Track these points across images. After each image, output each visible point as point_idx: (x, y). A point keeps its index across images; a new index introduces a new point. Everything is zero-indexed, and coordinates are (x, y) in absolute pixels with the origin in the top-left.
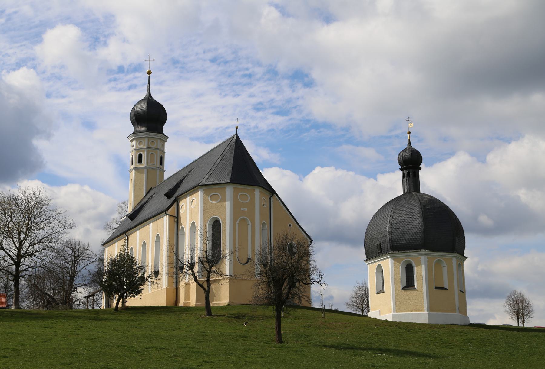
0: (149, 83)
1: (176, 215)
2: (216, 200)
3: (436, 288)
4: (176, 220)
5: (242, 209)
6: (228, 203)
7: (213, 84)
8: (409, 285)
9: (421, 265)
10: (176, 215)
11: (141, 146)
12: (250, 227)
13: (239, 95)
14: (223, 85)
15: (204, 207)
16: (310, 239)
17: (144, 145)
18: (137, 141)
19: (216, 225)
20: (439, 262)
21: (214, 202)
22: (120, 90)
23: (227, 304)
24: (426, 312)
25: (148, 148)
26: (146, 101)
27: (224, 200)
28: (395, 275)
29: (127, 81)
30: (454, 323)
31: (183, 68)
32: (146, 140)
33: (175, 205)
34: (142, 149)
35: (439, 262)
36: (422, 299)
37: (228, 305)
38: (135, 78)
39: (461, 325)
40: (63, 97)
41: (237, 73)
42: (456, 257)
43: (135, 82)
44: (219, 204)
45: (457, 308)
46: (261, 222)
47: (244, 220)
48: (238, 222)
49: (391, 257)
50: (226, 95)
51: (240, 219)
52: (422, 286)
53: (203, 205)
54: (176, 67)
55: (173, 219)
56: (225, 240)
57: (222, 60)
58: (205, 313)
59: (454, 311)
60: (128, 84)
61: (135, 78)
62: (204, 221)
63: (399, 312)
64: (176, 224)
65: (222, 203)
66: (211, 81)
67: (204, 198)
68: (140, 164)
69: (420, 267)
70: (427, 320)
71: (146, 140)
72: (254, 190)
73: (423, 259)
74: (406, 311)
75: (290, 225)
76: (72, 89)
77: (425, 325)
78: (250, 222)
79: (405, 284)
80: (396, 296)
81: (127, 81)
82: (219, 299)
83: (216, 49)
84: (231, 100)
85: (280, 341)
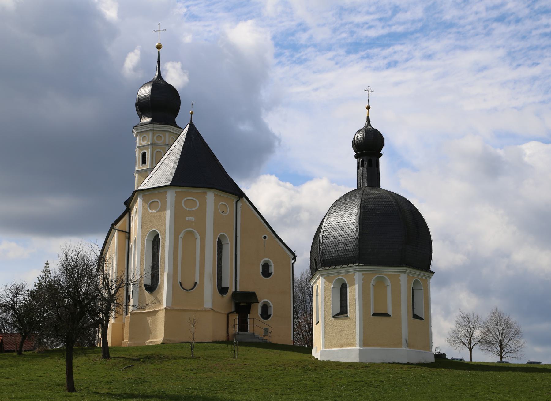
0: (159, 61)
1: (127, 231)
2: (155, 209)
3: (374, 315)
4: (127, 236)
5: (187, 219)
6: (168, 212)
7: (501, 52)
8: (343, 312)
9: (355, 284)
10: (127, 231)
11: (145, 143)
12: (198, 241)
13: (538, 64)
14: (514, 52)
15: (143, 217)
16: (293, 253)
17: (148, 141)
18: (140, 136)
19: (156, 241)
20: (380, 281)
21: (154, 211)
22: (377, 69)
23: (161, 341)
24: (358, 347)
25: (153, 144)
26: (151, 84)
27: (164, 209)
28: (325, 299)
29: (385, 58)
30: (400, 362)
31: (459, 33)
32: (150, 134)
33: (127, 216)
34: (145, 147)
35: (380, 281)
36: (355, 330)
37: (163, 343)
38: (395, 52)
39: (408, 364)
40: (304, 84)
41: (534, 33)
42: (405, 272)
43: (396, 57)
44: (158, 213)
45: (404, 341)
46: (215, 234)
47: (190, 233)
48: (182, 235)
49: (321, 275)
50: (519, 65)
51: (185, 231)
52: (355, 313)
53: (141, 216)
54: (450, 33)
55: (123, 235)
56: (164, 260)
57: (512, 17)
58: (101, 355)
59: (399, 344)
60: (386, 61)
61: (395, 52)
62: (142, 237)
63: (329, 347)
64: (127, 241)
65: (162, 213)
66: (498, 47)
67: (143, 206)
68: (144, 165)
69: (353, 287)
70: (358, 358)
71: (150, 134)
72: (206, 194)
73: (358, 276)
74: (334, 347)
75: (265, 237)
76: (314, 72)
77: (350, 365)
78: (198, 236)
79: (338, 310)
80: (325, 326)
81: (385, 58)
82: (155, 337)
83: (502, 5)
84: (527, 72)
85: (71, 388)
